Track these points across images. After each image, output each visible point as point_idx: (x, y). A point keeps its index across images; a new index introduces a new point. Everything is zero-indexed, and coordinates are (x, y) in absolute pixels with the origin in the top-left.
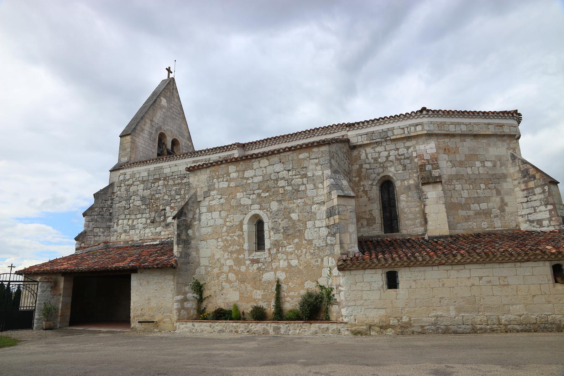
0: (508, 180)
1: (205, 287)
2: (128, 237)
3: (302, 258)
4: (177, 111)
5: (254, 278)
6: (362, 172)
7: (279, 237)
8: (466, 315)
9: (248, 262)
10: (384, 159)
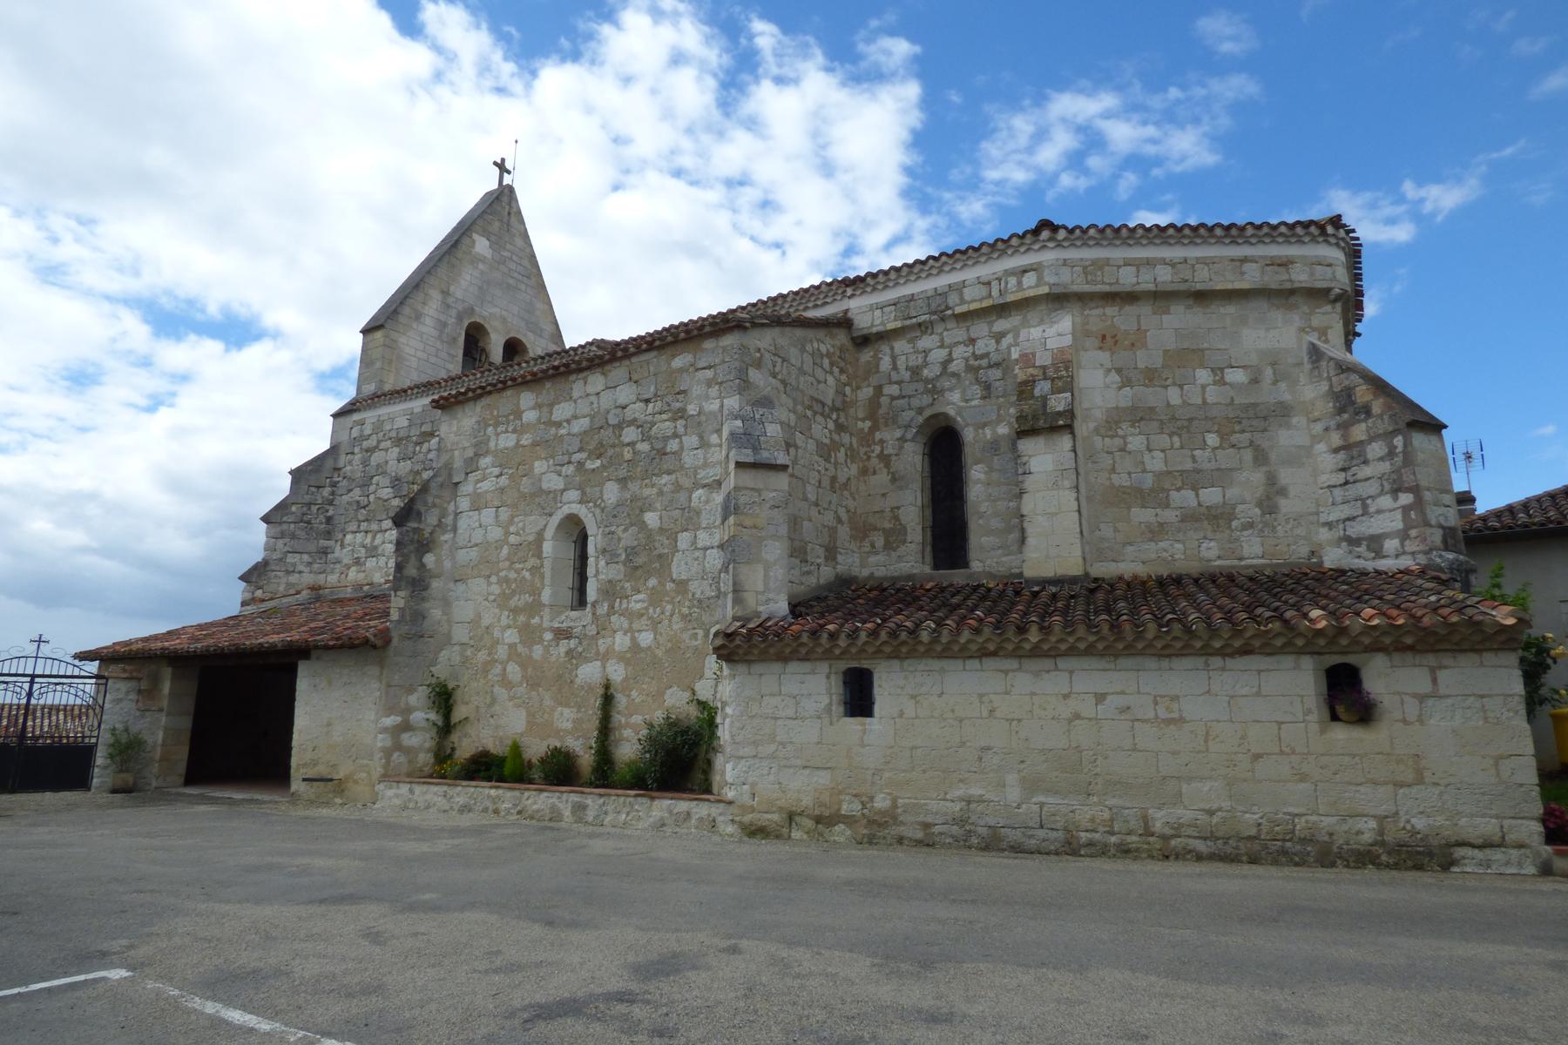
0: (1294, 420)
1: (458, 695)
2: (362, 575)
3: (662, 628)
4: (520, 268)
5: (560, 676)
6: (879, 405)
7: (615, 572)
8: (1050, 800)
9: (548, 636)
10: (937, 370)
